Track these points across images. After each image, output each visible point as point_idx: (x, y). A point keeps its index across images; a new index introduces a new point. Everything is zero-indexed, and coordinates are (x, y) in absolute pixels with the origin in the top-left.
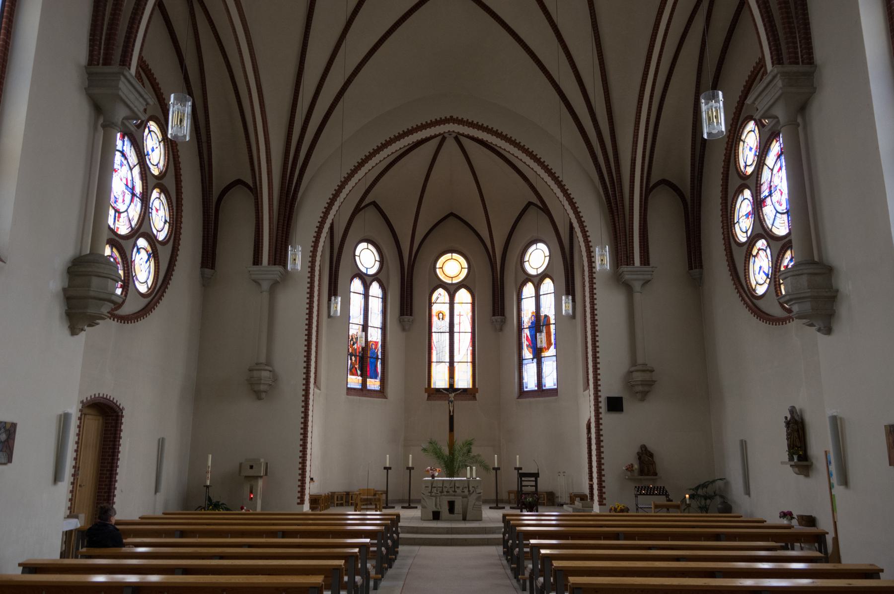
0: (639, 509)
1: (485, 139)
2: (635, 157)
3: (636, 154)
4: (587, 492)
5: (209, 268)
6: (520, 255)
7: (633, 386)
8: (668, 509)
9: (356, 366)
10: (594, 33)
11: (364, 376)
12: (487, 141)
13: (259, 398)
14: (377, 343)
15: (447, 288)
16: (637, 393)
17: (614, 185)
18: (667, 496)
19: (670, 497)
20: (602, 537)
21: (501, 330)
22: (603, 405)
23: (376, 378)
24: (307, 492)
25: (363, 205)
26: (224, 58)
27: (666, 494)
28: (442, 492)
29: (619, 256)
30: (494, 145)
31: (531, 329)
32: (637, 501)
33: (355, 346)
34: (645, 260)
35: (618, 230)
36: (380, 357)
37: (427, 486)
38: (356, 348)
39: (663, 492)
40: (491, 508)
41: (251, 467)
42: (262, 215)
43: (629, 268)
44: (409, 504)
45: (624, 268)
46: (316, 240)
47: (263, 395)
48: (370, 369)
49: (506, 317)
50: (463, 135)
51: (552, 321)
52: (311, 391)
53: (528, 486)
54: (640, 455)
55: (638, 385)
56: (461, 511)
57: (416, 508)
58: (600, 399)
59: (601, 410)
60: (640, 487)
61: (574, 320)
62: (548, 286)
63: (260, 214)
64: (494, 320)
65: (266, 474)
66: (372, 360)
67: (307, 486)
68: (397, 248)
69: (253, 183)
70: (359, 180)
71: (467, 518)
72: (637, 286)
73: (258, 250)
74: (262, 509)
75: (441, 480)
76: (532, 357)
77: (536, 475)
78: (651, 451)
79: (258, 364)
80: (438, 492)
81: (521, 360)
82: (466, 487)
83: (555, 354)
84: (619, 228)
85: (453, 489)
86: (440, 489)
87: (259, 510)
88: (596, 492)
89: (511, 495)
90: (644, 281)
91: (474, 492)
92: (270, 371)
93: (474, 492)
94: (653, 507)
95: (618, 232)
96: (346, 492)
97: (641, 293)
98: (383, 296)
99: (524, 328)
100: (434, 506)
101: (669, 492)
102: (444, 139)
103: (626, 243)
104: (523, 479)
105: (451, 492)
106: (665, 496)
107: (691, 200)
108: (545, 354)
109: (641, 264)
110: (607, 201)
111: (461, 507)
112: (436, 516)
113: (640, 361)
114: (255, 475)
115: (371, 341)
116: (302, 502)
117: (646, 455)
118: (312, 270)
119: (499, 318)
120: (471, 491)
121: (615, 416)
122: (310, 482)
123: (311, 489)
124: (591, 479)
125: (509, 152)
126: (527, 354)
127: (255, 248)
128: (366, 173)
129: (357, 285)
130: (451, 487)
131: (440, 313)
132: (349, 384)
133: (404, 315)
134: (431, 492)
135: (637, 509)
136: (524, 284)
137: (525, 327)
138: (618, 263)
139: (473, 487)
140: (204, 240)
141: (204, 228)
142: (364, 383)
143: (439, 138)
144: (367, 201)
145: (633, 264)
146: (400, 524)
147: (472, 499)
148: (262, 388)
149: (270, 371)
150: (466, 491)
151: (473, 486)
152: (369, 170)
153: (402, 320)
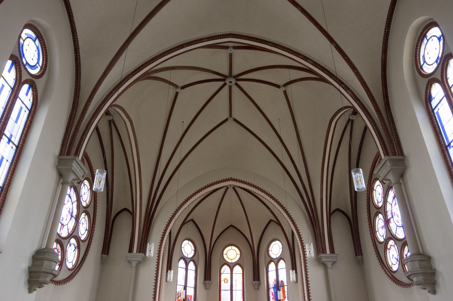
1: (248, 189)
2: (322, 198)
3: (322, 196)
5: (106, 254)
14: (191, 296)
21: (258, 289)
25: (187, 221)
29: (319, 248)
34: (332, 251)
35: (317, 234)
38: (180, 299)
42: (136, 226)
45: (321, 255)
46: (162, 239)
49: (260, 282)
50: (237, 186)
51: (285, 284)
61: (297, 284)
62: (282, 264)
63: (134, 226)
69: (132, 210)
70: (185, 208)
72: (329, 265)
95: (317, 235)
97: (332, 269)
102: (227, 188)
103: (321, 242)
109: (330, 253)
115: (188, 295)
129: (182, 263)
133: (206, 280)
136: (269, 263)
138: (318, 252)
140: (104, 239)
141: (105, 233)
143: (225, 188)
144: (189, 219)
145: (326, 253)
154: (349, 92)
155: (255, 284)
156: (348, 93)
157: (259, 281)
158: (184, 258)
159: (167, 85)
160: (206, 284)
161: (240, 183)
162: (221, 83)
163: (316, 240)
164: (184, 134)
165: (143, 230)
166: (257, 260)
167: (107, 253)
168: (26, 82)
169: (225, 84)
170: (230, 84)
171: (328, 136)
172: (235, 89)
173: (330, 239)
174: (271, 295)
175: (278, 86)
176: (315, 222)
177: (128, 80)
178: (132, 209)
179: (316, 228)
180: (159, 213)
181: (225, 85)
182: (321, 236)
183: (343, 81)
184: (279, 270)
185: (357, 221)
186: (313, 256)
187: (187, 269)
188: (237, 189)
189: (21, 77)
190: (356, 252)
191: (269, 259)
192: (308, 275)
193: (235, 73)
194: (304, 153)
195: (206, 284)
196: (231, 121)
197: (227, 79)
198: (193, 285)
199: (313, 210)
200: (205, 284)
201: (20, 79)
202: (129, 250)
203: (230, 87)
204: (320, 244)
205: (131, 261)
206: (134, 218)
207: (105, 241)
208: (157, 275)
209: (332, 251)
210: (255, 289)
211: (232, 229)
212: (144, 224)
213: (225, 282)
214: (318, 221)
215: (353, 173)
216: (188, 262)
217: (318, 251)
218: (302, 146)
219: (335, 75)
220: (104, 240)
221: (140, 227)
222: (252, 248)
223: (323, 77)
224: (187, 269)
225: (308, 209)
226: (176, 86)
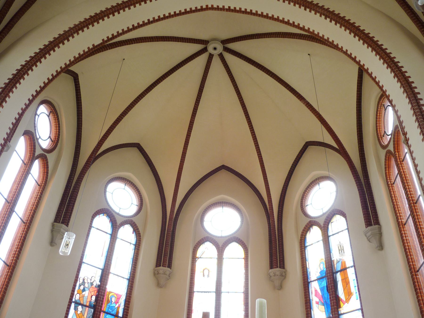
21: (281, 287)
31: (321, 280)
49: (286, 271)
61: (380, 252)
64: (271, 274)
68: (160, 194)
98: (136, 243)
115: (110, 292)
119: (277, 271)
131: (206, 269)
133: (160, 266)
155: (274, 276)
157: (284, 268)
160: (158, 273)
166: (278, 228)
168: (37, 158)
174: (314, 299)
187: (113, 237)
189: (34, 151)
191: (305, 221)
195: (158, 273)
198: (126, 272)
200: (156, 274)
201: (34, 154)
210: (275, 288)
213: (204, 276)
224: (113, 237)
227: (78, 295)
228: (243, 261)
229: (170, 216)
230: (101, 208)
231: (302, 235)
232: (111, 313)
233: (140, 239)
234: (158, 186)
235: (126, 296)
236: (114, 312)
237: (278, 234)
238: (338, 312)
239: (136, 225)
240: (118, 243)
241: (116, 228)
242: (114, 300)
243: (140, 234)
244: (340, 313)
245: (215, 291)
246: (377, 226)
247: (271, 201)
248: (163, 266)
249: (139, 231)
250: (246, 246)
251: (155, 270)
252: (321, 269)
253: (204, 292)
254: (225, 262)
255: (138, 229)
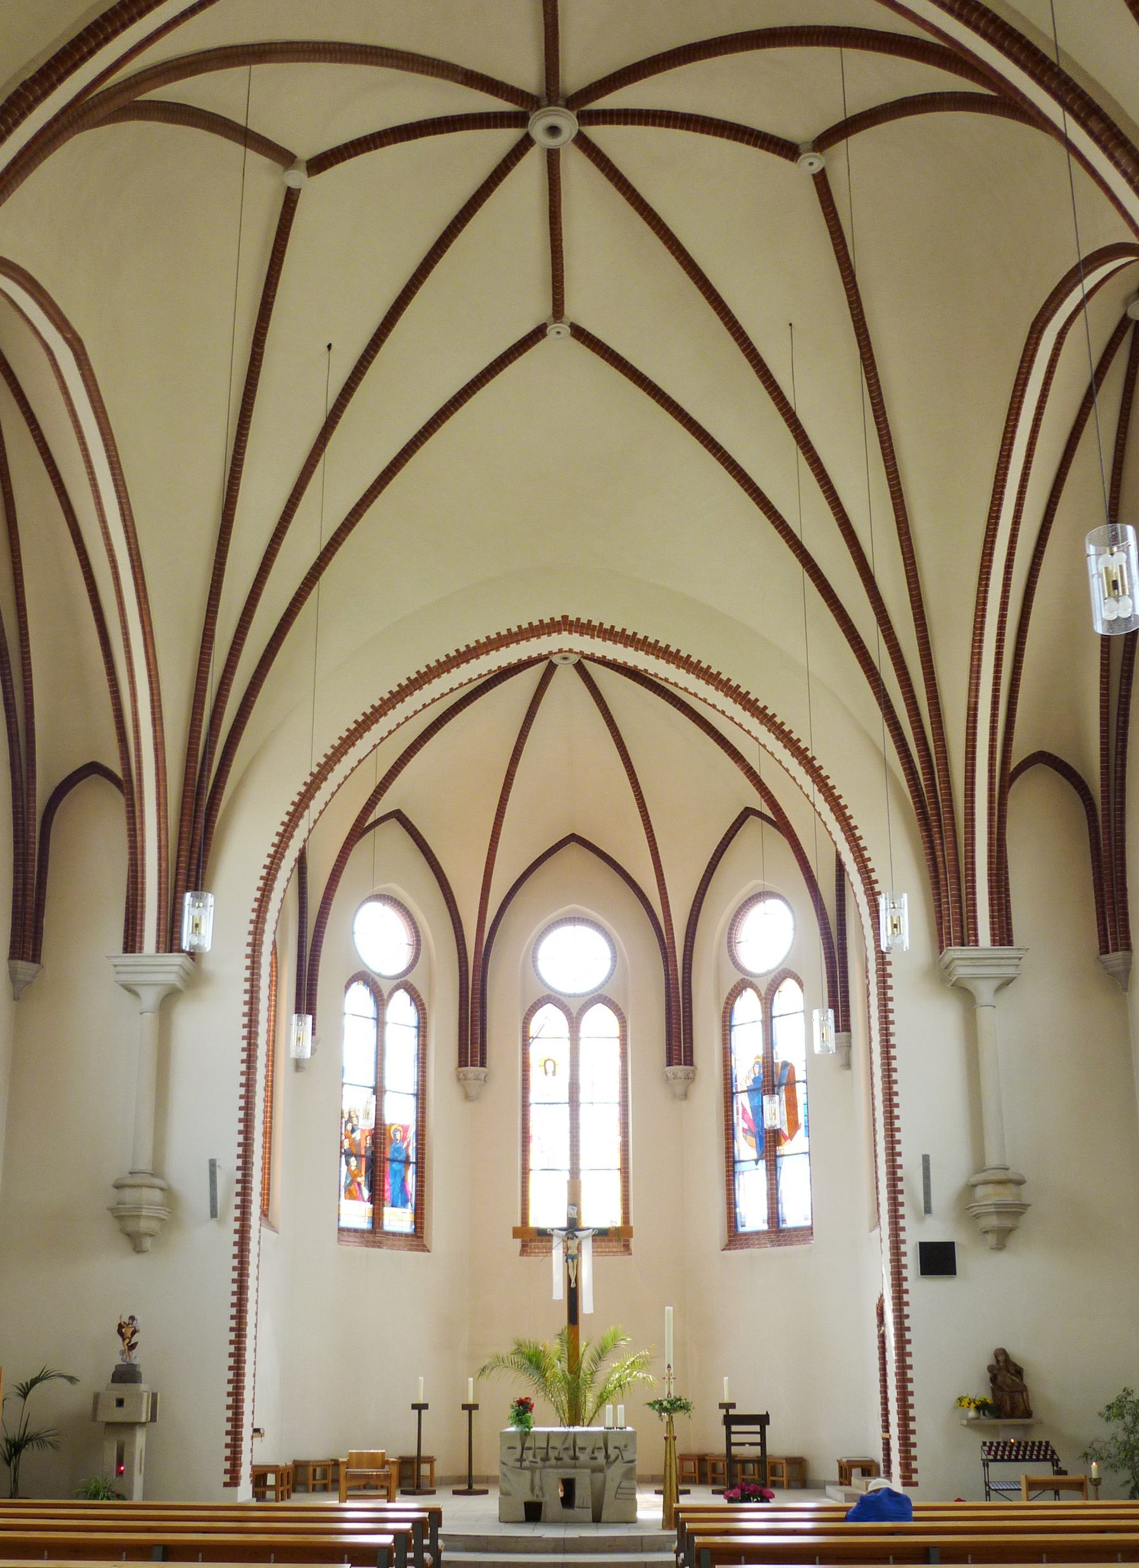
0: (992, 1493)
1: (641, 667)
2: (976, 703)
3: (977, 696)
4: (879, 1456)
5: (27, 960)
6: (726, 936)
7: (977, 1216)
8: (1057, 1493)
9: (359, 1179)
10: (865, 371)
11: (376, 1198)
12: (646, 671)
13: (138, 1249)
14: (405, 1129)
15: (563, 1003)
16: (986, 1232)
17: (931, 767)
18: (1055, 1462)
19: (1060, 1465)
20: (891, 1558)
21: (685, 1096)
22: (911, 1261)
23: (404, 1204)
24: (245, 1459)
25: (371, 820)
26: (59, 496)
27: (1052, 1457)
28: (546, 1459)
29: (945, 924)
30: (661, 679)
31: (754, 1093)
32: (986, 1474)
33: (357, 1135)
34: (1003, 934)
35: (941, 865)
36: (413, 1159)
37: (511, 1445)
38: (358, 1138)
39: (1044, 1452)
40: (455, 1493)
41: (120, 1403)
42: (143, 841)
43: (967, 952)
44: (469, 1485)
45: (955, 952)
46: (263, 896)
47: (148, 1243)
48: (390, 1187)
49: (696, 1068)
50: (592, 658)
51: (800, 1075)
52: (253, 1234)
53: (743, 1444)
54: (995, 1372)
55: (989, 1213)
56: (589, 1502)
57: (485, 1492)
58: (903, 1248)
59: (905, 1273)
60: (995, 1444)
61: (848, 1072)
62: (789, 996)
63: (139, 838)
65: (153, 1418)
66: (395, 1166)
67: (246, 1445)
68: (450, 911)
69: (123, 770)
70: (360, 762)
71: (604, 1518)
72: (984, 991)
73: (135, 918)
74: (145, 1497)
75: (544, 1432)
76: (755, 1156)
77: (762, 1420)
78: (1019, 1363)
79: (135, 1173)
80: (538, 1460)
81: (731, 1163)
82: (600, 1448)
83: (808, 1151)
84: (944, 862)
85: (572, 1452)
86: (541, 1454)
87: (137, 1498)
88: (895, 1457)
89: (686, 1463)
90: (1000, 982)
91: (617, 1458)
92: (162, 1189)
93: (617, 1458)
94: (1023, 1487)
95: (941, 871)
96: (332, 1460)
99: (737, 1092)
100: (529, 1492)
101: (1060, 1454)
102: (551, 668)
103: (960, 896)
104: (734, 1428)
105: (567, 1460)
106: (1049, 1464)
107: (1103, 797)
108: (785, 1148)
109: (994, 942)
110: (915, 803)
111: (589, 1493)
112: (533, 1513)
113: (992, 1160)
114: (130, 1420)
115: (392, 1125)
116: (234, 1481)
117: (1008, 1371)
118: (253, 962)
119: (679, 1070)
120: (613, 1457)
121: (938, 1285)
122: (252, 1437)
123: (254, 1453)
124: (886, 1427)
125: (696, 695)
126: (746, 1148)
127: (127, 914)
128: (375, 746)
129: (359, 998)
130: (566, 1449)
131: (549, 1060)
132: (342, 1218)
134: (521, 1460)
135: (988, 1494)
136: (736, 992)
137: (739, 1090)
138: (941, 942)
139: (615, 1448)
140: (15, 896)
141: (16, 871)
142: (377, 1218)
143: (540, 668)
144: (379, 811)
145: (976, 942)
146: (440, 1531)
147: (615, 1473)
148: (144, 1225)
149: (162, 1189)
150: (600, 1456)
151: (617, 1444)
152: (382, 739)
153: (461, 1076)
154: (1123, 162)
156: (1117, 165)
157: (692, 1065)
158: (364, 977)
159: (233, 149)
161: (604, 640)
162: (508, 137)
163: (938, 888)
164: (335, 406)
165: (178, 857)
166: (683, 978)
167: (34, 956)
169: (526, 143)
170: (552, 143)
171: (1019, 408)
172: (575, 165)
173: (998, 887)
175: (788, 150)
176: (938, 815)
177: (23, 116)
178: (122, 764)
179: (941, 838)
180: (241, 784)
181: (527, 150)
182: (958, 872)
183: (1098, 100)
184: (774, 1020)
185: (1123, 803)
186: (907, 944)
187: (380, 1022)
188: (597, 672)
190: (1106, 936)
192: (892, 1034)
193: (573, 78)
194: (901, 496)
196: (558, 340)
197: (533, 117)
199: (930, 761)
200: (461, 1079)
202: (126, 943)
203: (553, 158)
204: (954, 907)
205: (134, 987)
206: (133, 806)
207: (19, 904)
208: (249, 1044)
209: (1003, 934)
211: (573, 854)
212: (181, 832)
213: (546, 1073)
214: (951, 806)
215: (1091, 549)
216: (385, 993)
217: (940, 935)
218: (894, 458)
219: (1052, 56)
220: (15, 901)
221: (163, 843)
222: (661, 931)
223: (1015, 90)
224: (380, 1022)
225: (910, 756)
226: (284, 157)
227: (347, 1140)
228: (617, 1042)
229: (475, 962)
230: (356, 972)
231: (727, 1003)
232: (399, 1159)
233: (425, 1014)
234: (445, 895)
235: (417, 1126)
236: (402, 1157)
237: (683, 995)
238: (775, 1151)
239: (414, 988)
240: (389, 1030)
241: (383, 1005)
242: (398, 1136)
243: (423, 1005)
244: (778, 1154)
245: (568, 1101)
246: (845, 1033)
247: (672, 929)
248: (471, 1066)
249: (421, 1000)
250: (622, 1014)
251: (459, 1072)
252: (755, 1074)
253: (549, 1104)
254: (583, 1045)
255: (419, 996)
